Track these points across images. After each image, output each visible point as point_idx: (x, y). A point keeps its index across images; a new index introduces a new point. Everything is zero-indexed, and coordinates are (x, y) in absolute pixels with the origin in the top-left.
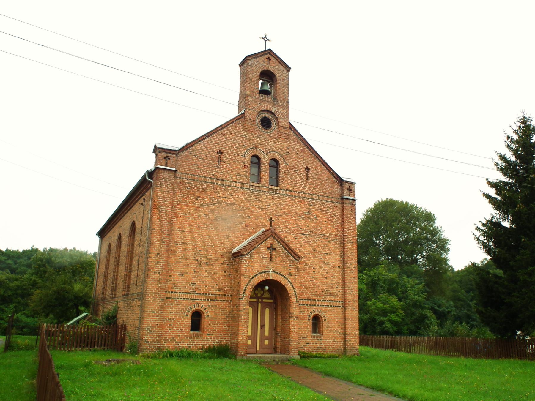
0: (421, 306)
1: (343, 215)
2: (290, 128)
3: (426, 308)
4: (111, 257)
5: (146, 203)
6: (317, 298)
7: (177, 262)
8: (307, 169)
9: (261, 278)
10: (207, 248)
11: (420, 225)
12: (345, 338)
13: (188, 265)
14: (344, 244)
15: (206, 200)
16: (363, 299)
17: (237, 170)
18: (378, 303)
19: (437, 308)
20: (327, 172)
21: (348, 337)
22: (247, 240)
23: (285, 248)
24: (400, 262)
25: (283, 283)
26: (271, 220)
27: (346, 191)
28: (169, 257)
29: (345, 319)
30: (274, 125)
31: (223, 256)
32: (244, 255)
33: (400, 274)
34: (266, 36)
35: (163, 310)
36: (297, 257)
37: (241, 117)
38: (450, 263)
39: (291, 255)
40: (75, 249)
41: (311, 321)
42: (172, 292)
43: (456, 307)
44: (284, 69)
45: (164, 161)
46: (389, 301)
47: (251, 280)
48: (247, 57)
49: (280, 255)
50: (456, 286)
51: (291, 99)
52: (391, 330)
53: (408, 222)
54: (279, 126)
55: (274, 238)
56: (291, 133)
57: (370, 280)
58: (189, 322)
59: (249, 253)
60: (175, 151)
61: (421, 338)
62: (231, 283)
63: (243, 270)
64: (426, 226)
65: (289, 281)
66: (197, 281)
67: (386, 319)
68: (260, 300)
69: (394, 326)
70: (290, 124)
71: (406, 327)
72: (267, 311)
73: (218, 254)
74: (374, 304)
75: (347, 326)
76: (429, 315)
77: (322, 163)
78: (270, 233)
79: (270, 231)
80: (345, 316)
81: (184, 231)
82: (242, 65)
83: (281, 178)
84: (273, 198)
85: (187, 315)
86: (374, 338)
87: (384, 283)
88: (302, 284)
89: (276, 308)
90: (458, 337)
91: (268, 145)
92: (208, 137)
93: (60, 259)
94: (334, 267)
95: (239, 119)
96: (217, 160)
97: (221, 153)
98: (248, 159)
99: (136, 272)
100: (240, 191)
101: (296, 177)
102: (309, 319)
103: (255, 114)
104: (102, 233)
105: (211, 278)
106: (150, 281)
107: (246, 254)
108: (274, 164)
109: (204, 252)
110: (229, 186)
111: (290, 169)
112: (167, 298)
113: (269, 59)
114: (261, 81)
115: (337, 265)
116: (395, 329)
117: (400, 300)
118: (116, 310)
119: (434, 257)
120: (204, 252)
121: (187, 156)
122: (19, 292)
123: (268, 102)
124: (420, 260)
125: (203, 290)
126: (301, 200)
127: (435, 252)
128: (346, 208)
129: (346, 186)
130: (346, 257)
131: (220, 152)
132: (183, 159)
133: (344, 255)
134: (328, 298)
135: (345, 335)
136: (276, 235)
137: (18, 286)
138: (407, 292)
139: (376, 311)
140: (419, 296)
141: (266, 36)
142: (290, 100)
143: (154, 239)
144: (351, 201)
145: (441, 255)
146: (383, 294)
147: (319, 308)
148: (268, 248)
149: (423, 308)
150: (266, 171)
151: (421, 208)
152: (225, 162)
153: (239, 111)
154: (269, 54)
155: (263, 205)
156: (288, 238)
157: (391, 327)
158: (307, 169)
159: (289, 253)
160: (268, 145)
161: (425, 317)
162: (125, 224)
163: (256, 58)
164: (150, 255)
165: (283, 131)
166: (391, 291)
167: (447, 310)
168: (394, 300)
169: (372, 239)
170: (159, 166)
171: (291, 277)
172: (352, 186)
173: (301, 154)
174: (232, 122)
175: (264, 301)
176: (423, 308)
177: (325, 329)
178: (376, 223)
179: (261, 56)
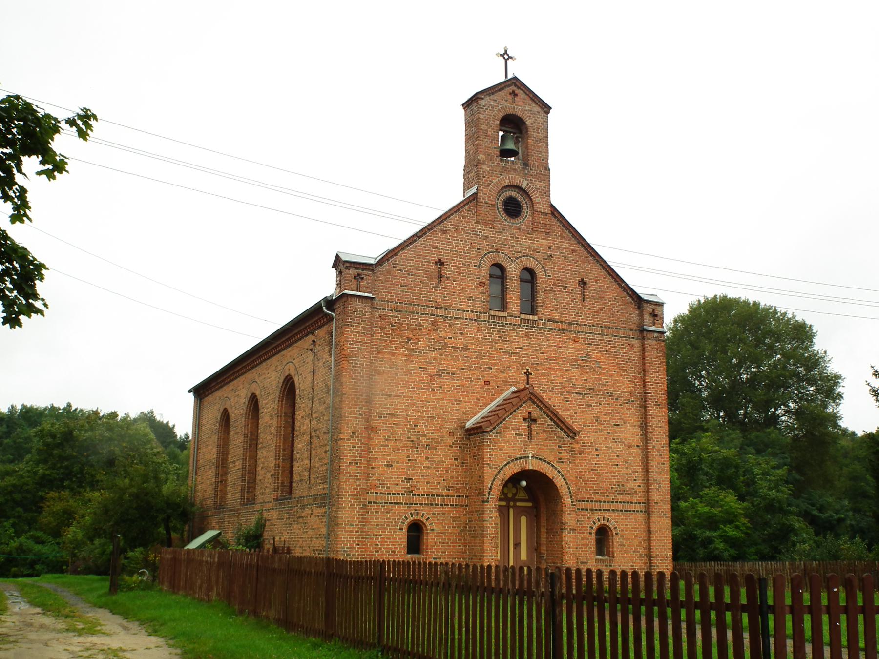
0: (781, 510)
1: (643, 359)
2: (553, 214)
3: (790, 512)
4: (232, 433)
5: (317, 348)
6: (603, 499)
7: (381, 445)
8: (583, 283)
9: (515, 468)
10: (427, 420)
11: (782, 349)
12: (650, 563)
13: (399, 449)
14: (645, 407)
15: (421, 344)
16: (676, 497)
17: (467, 291)
18: (700, 505)
19: (815, 512)
20: (615, 286)
21: (654, 561)
22: (489, 407)
23: (551, 419)
24: (742, 423)
25: (550, 476)
26: (528, 374)
27: (647, 318)
28: (370, 438)
29: (649, 532)
30: (526, 210)
31: (451, 434)
32: (487, 432)
33: (741, 448)
34: (506, 51)
35: (364, 521)
36: (572, 433)
37: (471, 201)
38: (843, 424)
39: (562, 429)
40: (69, 405)
41: (594, 536)
42: (377, 493)
43: (856, 510)
44: (540, 110)
45: (354, 282)
46: (722, 500)
47: (499, 472)
48: (477, 94)
49: (544, 431)
50: (858, 466)
51: (553, 163)
52: (726, 554)
53: (759, 342)
54: (534, 211)
55: (534, 403)
56: (554, 221)
57: (684, 461)
58: (404, 539)
59: (495, 428)
60: (371, 265)
61: (779, 565)
62: (466, 477)
63: (487, 456)
64: (794, 349)
65: (559, 472)
66: (413, 475)
67: (715, 534)
68: (512, 504)
69: (731, 547)
70: (552, 206)
71: (753, 550)
72: (523, 520)
73: (443, 431)
74: (693, 506)
75: (653, 544)
76: (797, 525)
77: (607, 271)
78: (527, 395)
79: (527, 392)
80: (649, 527)
81: (390, 396)
82: (468, 106)
83: (539, 300)
84: (527, 336)
85: (401, 529)
86: (696, 567)
87: (711, 466)
88: (580, 476)
89: (537, 517)
90: (844, 560)
91: (517, 245)
92: (419, 237)
93: (89, 434)
94: (629, 446)
95: (467, 204)
96: (435, 274)
97: (442, 264)
98: (485, 271)
99: (307, 462)
100: (473, 326)
101: (564, 297)
102: (590, 533)
103: (494, 194)
104: (202, 391)
105: (435, 471)
106: (343, 477)
107: (491, 431)
108: (527, 276)
109: (422, 428)
110: (456, 318)
111: (554, 284)
112: (370, 503)
113: (514, 94)
114: (501, 133)
115: (635, 443)
116: (733, 552)
117: (741, 498)
118: (261, 525)
119: (812, 412)
120: (422, 428)
121: (389, 272)
122: (17, 496)
123: (515, 170)
124: (783, 418)
125: (423, 488)
126: (573, 336)
127: (813, 401)
128: (648, 347)
129: (648, 308)
130: (650, 430)
131: (440, 262)
132: (382, 278)
133: (646, 426)
134: (620, 498)
135: (650, 558)
136: (536, 397)
137: (14, 486)
138: (754, 483)
139: (697, 520)
140: (778, 491)
141: (506, 51)
142: (551, 166)
143: (346, 411)
144: (656, 335)
145: (826, 407)
146: (709, 487)
147: (607, 515)
148: (525, 419)
149: (786, 513)
150: (515, 290)
151: (786, 313)
152: (448, 278)
153: (466, 188)
154: (513, 86)
155: (512, 347)
156: (553, 400)
157: (726, 550)
158: (583, 283)
159: (558, 426)
160: (517, 245)
161: (790, 530)
162: (267, 379)
163: (493, 94)
164: (341, 436)
165: (541, 219)
166: (725, 482)
167: (836, 517)
168: (730, 499)
169: (685, 378)
170: (347, 292)
171: (562, 465)
172: (659, 308)
173: (572, 257)
174: (457, 209)
175: (518, 504)
176: (786, 513)
177: (616, 549)
178: (694, 346)
179: (500, 90)
